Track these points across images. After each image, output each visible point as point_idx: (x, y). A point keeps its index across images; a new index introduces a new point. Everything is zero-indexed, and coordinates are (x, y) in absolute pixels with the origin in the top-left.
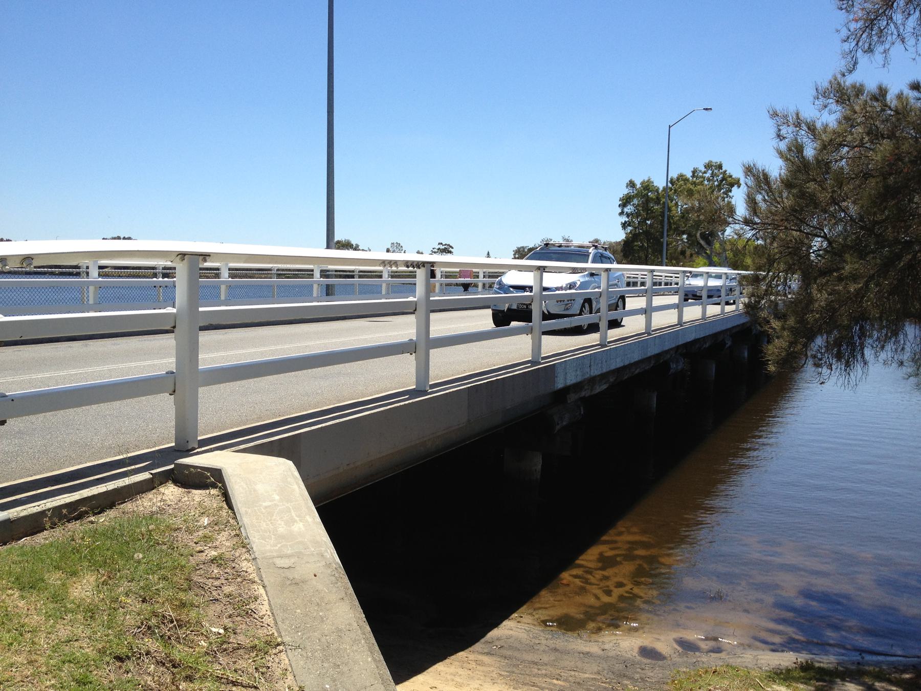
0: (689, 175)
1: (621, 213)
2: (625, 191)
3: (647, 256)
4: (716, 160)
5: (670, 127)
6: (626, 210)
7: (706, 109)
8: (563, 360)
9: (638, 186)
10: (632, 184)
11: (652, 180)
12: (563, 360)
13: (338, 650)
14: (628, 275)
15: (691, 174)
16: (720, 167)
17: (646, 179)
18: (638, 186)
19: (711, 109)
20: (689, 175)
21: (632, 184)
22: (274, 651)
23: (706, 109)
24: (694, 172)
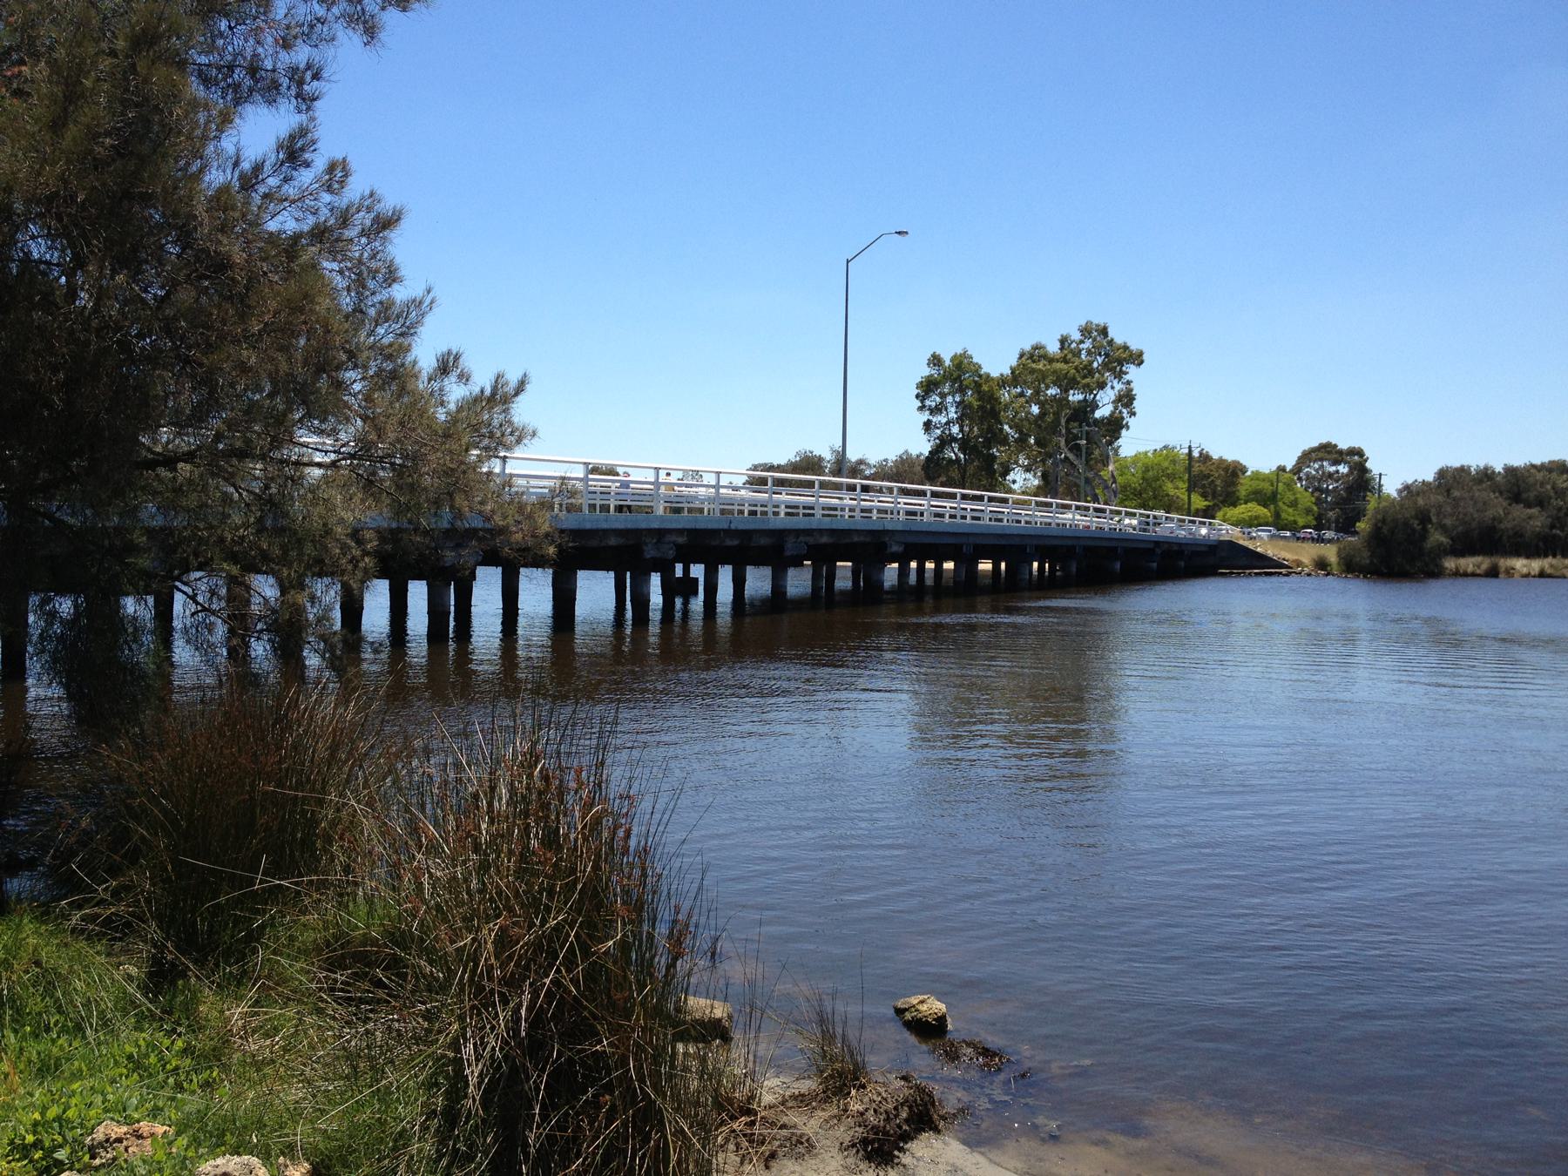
0: (1053, 348)
1: (921, 408)
2: (926, 371)
3: (963, 477)
4: (1098, 320)
5: (848, 262)
6: (928, 403)
7: (899, 233)
8: (629, 614)
9: (947, 363)
10: (935, 360)
11: (969, 353)
12: (629, 614)
13: (31, 880)
14: (1103, 515)
15: (1058, 345)
16: (1104, 331)
17: (960, 351)
18: (947, 363)
19: (906, 233)
20: (1053, 348)
21: (935, 360)
22: (1208, 1100)
23: (899, 233)
24: (1064, 341)
